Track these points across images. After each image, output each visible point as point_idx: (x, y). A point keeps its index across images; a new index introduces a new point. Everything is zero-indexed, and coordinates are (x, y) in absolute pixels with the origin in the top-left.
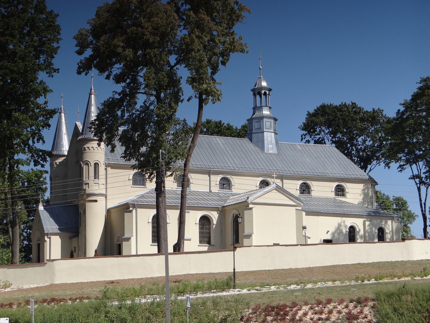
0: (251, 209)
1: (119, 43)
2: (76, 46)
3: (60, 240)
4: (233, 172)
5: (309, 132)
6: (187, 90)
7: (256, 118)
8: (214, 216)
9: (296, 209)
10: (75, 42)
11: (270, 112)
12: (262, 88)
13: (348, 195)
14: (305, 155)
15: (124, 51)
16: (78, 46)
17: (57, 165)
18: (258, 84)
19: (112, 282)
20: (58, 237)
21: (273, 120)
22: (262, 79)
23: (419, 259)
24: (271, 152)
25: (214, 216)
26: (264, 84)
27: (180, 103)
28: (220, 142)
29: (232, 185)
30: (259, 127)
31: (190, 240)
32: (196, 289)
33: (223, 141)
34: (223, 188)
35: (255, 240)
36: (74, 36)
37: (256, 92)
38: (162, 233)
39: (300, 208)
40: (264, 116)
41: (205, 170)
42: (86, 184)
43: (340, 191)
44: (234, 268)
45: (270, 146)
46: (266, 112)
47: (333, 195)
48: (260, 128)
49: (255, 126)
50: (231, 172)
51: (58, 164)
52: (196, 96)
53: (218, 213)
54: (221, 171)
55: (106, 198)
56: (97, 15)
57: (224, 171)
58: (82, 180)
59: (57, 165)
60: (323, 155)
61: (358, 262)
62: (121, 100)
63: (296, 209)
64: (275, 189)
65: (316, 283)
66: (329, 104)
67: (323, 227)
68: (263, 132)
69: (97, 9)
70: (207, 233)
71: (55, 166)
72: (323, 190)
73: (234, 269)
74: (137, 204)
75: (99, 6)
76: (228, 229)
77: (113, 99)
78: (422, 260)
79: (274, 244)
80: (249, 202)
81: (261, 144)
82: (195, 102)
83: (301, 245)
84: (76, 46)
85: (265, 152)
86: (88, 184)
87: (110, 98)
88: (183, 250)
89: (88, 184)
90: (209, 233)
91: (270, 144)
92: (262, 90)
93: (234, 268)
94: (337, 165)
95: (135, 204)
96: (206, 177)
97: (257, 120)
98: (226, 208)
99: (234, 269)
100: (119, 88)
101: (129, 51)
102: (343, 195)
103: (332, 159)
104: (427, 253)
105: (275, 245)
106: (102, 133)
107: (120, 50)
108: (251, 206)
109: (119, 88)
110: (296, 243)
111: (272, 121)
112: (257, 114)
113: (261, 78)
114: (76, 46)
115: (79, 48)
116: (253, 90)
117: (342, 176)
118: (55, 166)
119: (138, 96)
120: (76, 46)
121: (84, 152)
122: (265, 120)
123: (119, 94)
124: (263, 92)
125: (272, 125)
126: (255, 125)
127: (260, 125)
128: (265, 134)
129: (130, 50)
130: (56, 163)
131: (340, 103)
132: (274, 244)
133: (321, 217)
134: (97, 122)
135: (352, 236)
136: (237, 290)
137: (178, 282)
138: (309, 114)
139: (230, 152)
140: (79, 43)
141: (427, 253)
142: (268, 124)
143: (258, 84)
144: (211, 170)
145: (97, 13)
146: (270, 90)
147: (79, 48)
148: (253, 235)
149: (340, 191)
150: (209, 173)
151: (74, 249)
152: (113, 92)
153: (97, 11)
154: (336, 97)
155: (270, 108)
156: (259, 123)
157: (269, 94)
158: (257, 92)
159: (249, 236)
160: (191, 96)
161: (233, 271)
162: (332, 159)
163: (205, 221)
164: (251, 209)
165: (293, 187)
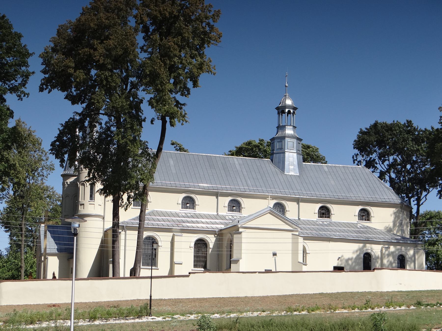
0: (240, 233)
1: (79, 63)
2: (42, 64)
3: (58, 261)
4: (243, 194)
5: (361, 151)
6: (148, 112)
7: (278, 138)
8: (211, 240)
9: (293, 234)
10: (41, 60)
11: (294, 131)
12: (285, 107)
13: (372, 219)
14: (330, 177)
15: (75, 72)
16: (44, 65)
17: (68, 184)
18: (283, 102)
19: (54, 306)
20: (56, 258)
21: (295, 140)
22: (287, 96)
23: (390, 290)
24: (292, 173)
25: (211, 240)
26: (289, 102)
27: (143, 123)
28: (236, 163)
29: (242, 208)
30: (280, 147)
31: (182, 264)
32: (109, 315)
33: (241, 162)
34: (233, 211)
35: (243, 265)
36: (40, 55)
37: (280, 110)
38: (116, 257)
39: (297, 233)
40: (286, 135)
41: (212, 192)
42: (81, 205)
43: (365, 215)
44: (151, 295)
45: (292, 167)
46: (289, 131)
47: (355, 220)
48: (281, 149)
49: (276, 146)
50: (240, 193)
51: (69, 183)
52: (158, 118)
53: (215, 237)
54: (231, 193)
55: (104, 218)
56: (59, 33)
57: (234, 193)
58: (79, 201)
59: (68, 184)
60: (350, 177)
61: (321, 292)
62: (82, 121)
63: (293, 234)
64: (269, 213)
65: (241, 312)
66: (382, 122)
67: (327, 254)
68: (284, 153)
69: (58, 28)
70: (202, 257)
71: (66, 186)
72: (345, 215)
73: (151, 297)
74: (126, 226)
75: (60, 25)
76: (215, 255)
77: (73, 119)
78: (439, 290)
79: (265, 270)
80: (239, 226)
81: (281, 165)
82: (158, 123)
83: (259, 272)
84: (42, 64)
85: (285, 173)
86: (83, 204)
87: (71, 118)
88: (139, 275)
89: (83, 204)
90: (206, 257)
91: (292, 165)
92: (286, 108)
93: (151, 295)
94: (364, 187)
95: (123, 226)
96: (214, 198)
97: (279, 140)
98: (223, 232)
99: (151, 297)
100: (80, 108)
101: (80, 72)
102: (368, 220)
103: (361, 181)
104: (401, 284)
105: (268, 271)
106: (63, 155)
107: (71, 71)
108: (241, 230)
109: (80, 108)
110: (291, 271)
111: (295, 141)
112: (280, 134)
113: (286, 96)
114: (42, 64)
115: (44, 66)
116: (277, 108)
117: (367, 200)
118: (66, 186)
119: (101, 116)
120: (42, 64)
121: (81, 172)
122: (287, 139)
123: (80, 114)
124: (287, 110)
125: (295, 145)
126: (277, 145)
127: (282, 145)
128: (287, 154)
129: (81, 71)
130: (67, 183)
131: (392, 122)
132: (265, 270)
133: (135, 249)
134: (58, 143)
135: (367, 263)
136: (152, 317)
137: (115, 307)
138: (361, 132)
139: (245, 173)
140: (45, 62)
141: (401, 284)
142: (290, 144)
143: (283, 102)
144: (218, 192)
145: (58, 32)
146: (295, 109)
147: (44, 66)
148: (241, 261)
149: (365, 215)
150: (217, 195)
151: (67, 272)
152: (74, 113)
153: (58, 30)
154: (391, 114)
155: (295, 127)
156: (281, 143)
157: (294, 112)
158: (281, 110)
159: (237, 261)
160: (153, 118)
161: (149, 298)
162: (361, 181)
163: (201, 244)
164: (240, 233)
165: (310, 212)
